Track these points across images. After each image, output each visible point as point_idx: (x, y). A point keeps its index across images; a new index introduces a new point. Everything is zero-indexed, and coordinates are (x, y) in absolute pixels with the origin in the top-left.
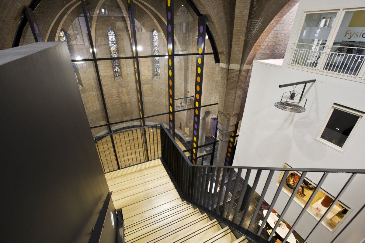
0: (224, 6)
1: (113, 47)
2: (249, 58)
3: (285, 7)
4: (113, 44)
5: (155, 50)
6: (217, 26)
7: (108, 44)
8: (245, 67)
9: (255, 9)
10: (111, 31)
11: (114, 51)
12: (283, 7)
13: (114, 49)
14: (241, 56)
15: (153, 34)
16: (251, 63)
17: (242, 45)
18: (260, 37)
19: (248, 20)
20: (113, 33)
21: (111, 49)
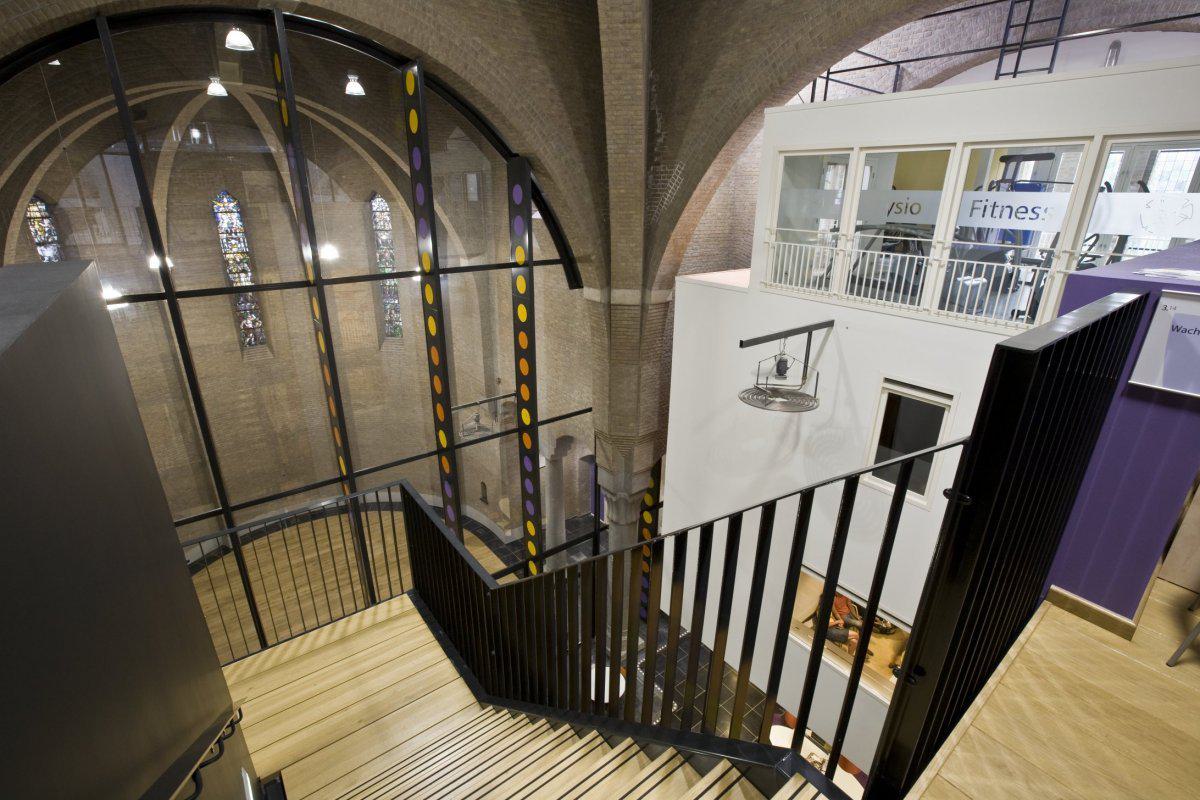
0: (577, 132)
1: (235, 250)
2: (663, 269)
3: (735, 137)
4: (233, 242)
5: (381, 256)
6: (562, 187)
7: (217, 241)
8: (656, 295)
9: (660, 140)
10: (225, 200)
11: (239, 263)
12: (728, 137)
13: (239, 257)
14: (639, 265)
15: (371, 206)
16: (670, 284)
17: (428, 411)
18: (685, 214)
19: (648, 169)
20: (232, 205)
21: (228, 256)
